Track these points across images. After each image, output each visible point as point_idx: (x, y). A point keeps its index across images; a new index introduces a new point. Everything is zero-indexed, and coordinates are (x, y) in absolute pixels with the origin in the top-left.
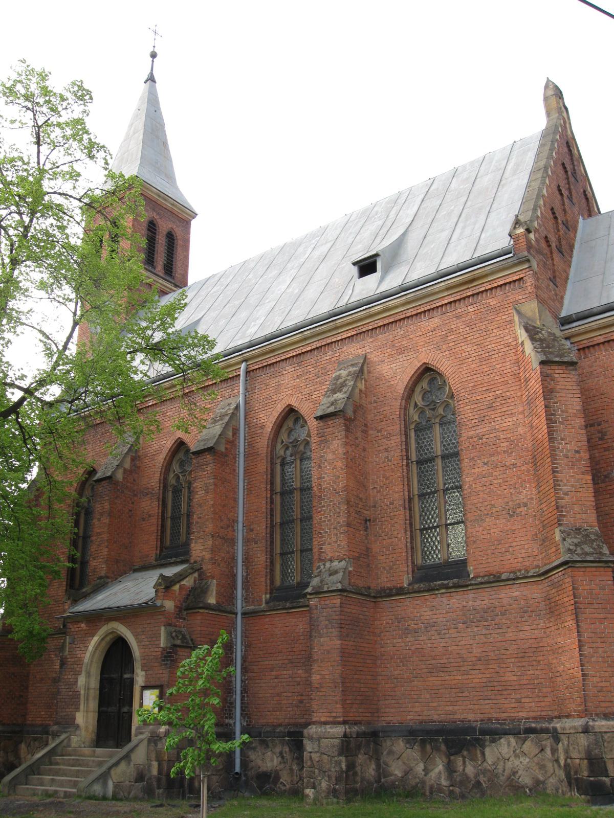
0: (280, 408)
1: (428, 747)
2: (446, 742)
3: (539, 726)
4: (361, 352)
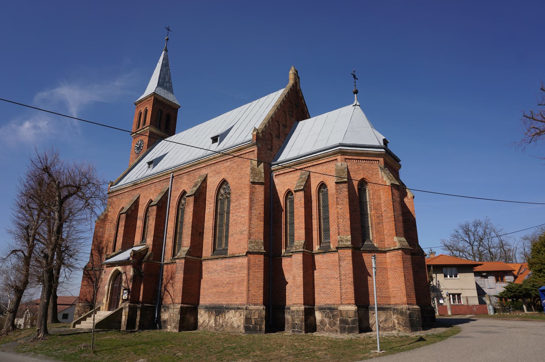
0: (181, 190)
2: (215, 311)
4: (206, 172)
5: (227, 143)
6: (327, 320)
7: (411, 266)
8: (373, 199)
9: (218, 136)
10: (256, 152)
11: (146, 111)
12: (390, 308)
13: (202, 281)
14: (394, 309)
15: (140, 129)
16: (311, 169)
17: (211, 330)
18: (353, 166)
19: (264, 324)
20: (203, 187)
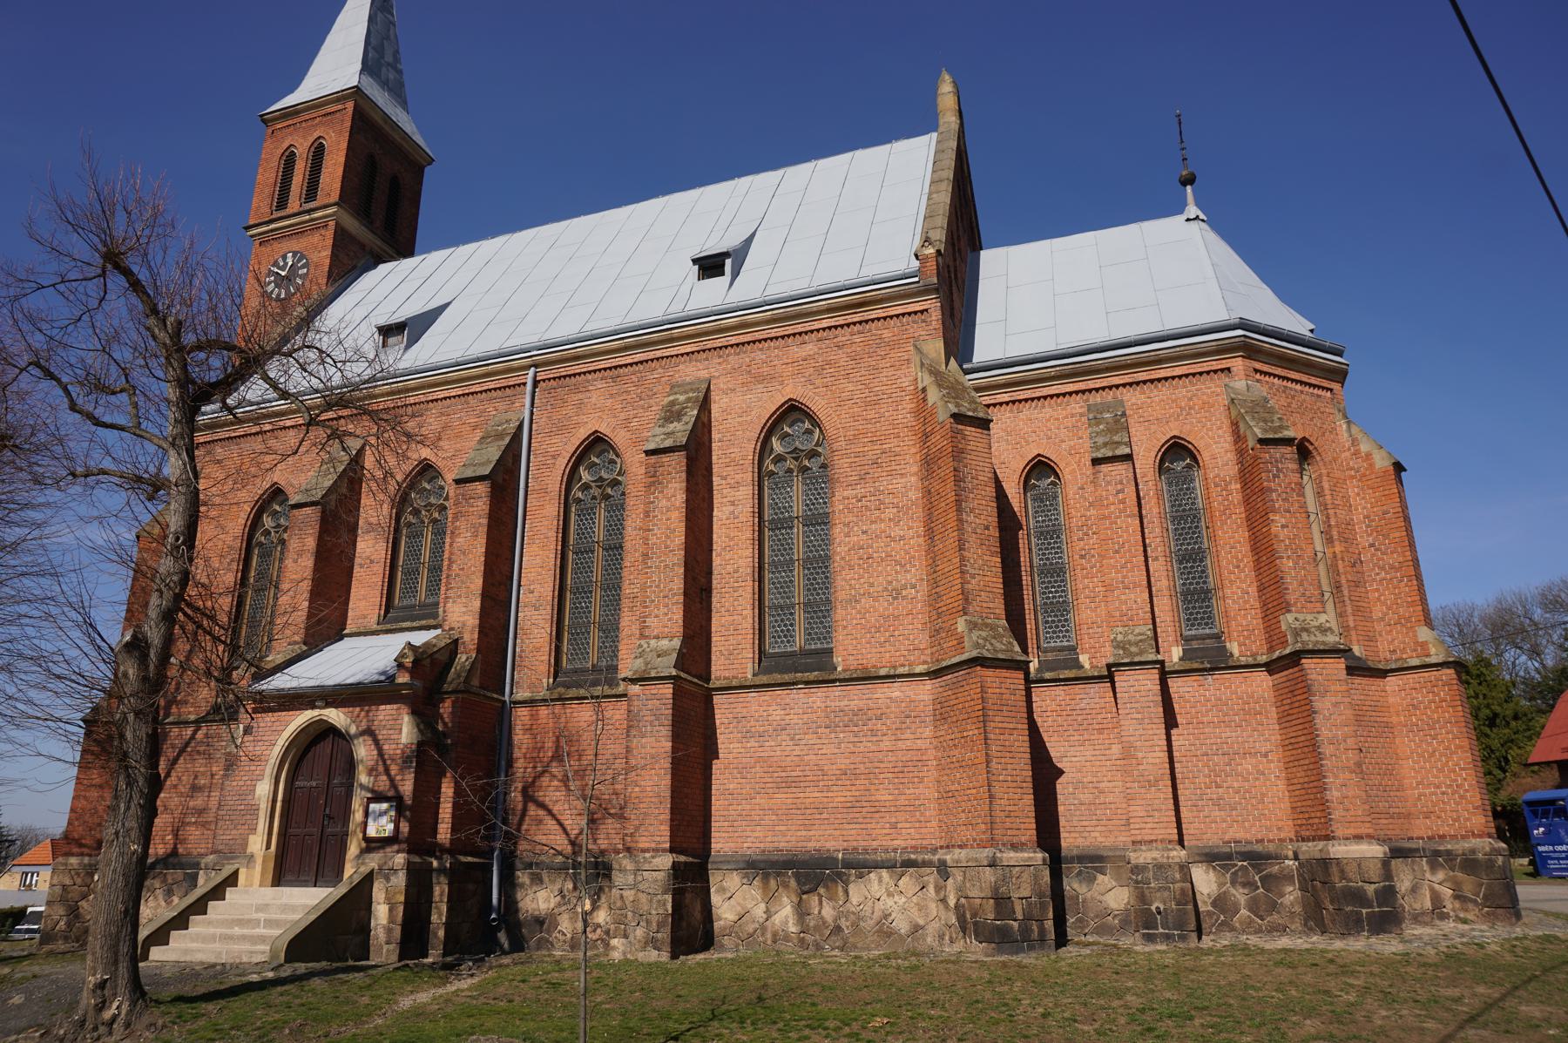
0: (583, 433)
1: (773, 883)
2: (797, 876)
3: (920, 858)
4: (704, 374)
5: (749, 286)
6: (1240, 895)
8: (1335, 507)
9: (726, 255)
10: (936, 315)
11: (318, 153)
12: (1417, 850)
13: (717, 766)
14: (1437, 853)
16: (1131, 397)
17: (781, 946)
19: (1051, 915)
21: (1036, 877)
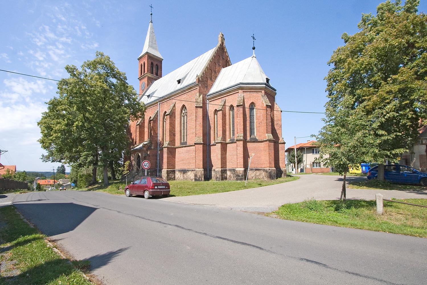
7: (273, 149)
10: (198, 89)
15: (142, 75)
16: (226, 98)
18: (247, 95)
20: (174, 109)
21: (201, 172)
